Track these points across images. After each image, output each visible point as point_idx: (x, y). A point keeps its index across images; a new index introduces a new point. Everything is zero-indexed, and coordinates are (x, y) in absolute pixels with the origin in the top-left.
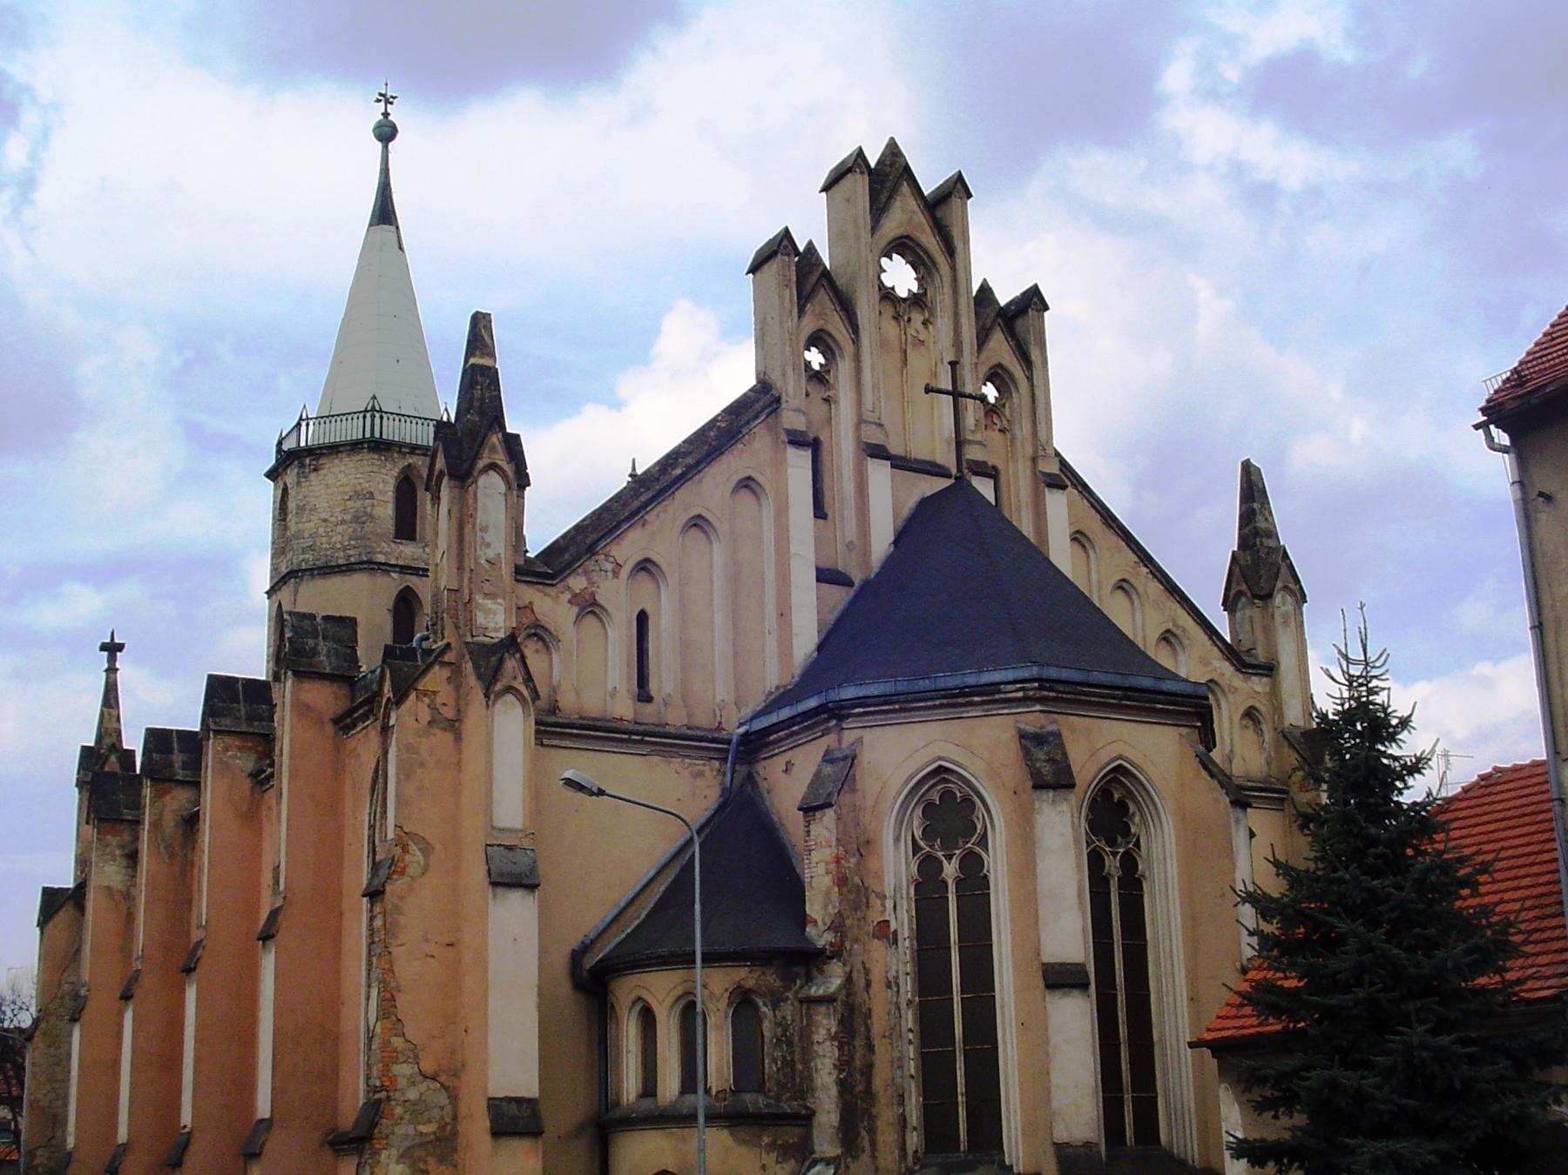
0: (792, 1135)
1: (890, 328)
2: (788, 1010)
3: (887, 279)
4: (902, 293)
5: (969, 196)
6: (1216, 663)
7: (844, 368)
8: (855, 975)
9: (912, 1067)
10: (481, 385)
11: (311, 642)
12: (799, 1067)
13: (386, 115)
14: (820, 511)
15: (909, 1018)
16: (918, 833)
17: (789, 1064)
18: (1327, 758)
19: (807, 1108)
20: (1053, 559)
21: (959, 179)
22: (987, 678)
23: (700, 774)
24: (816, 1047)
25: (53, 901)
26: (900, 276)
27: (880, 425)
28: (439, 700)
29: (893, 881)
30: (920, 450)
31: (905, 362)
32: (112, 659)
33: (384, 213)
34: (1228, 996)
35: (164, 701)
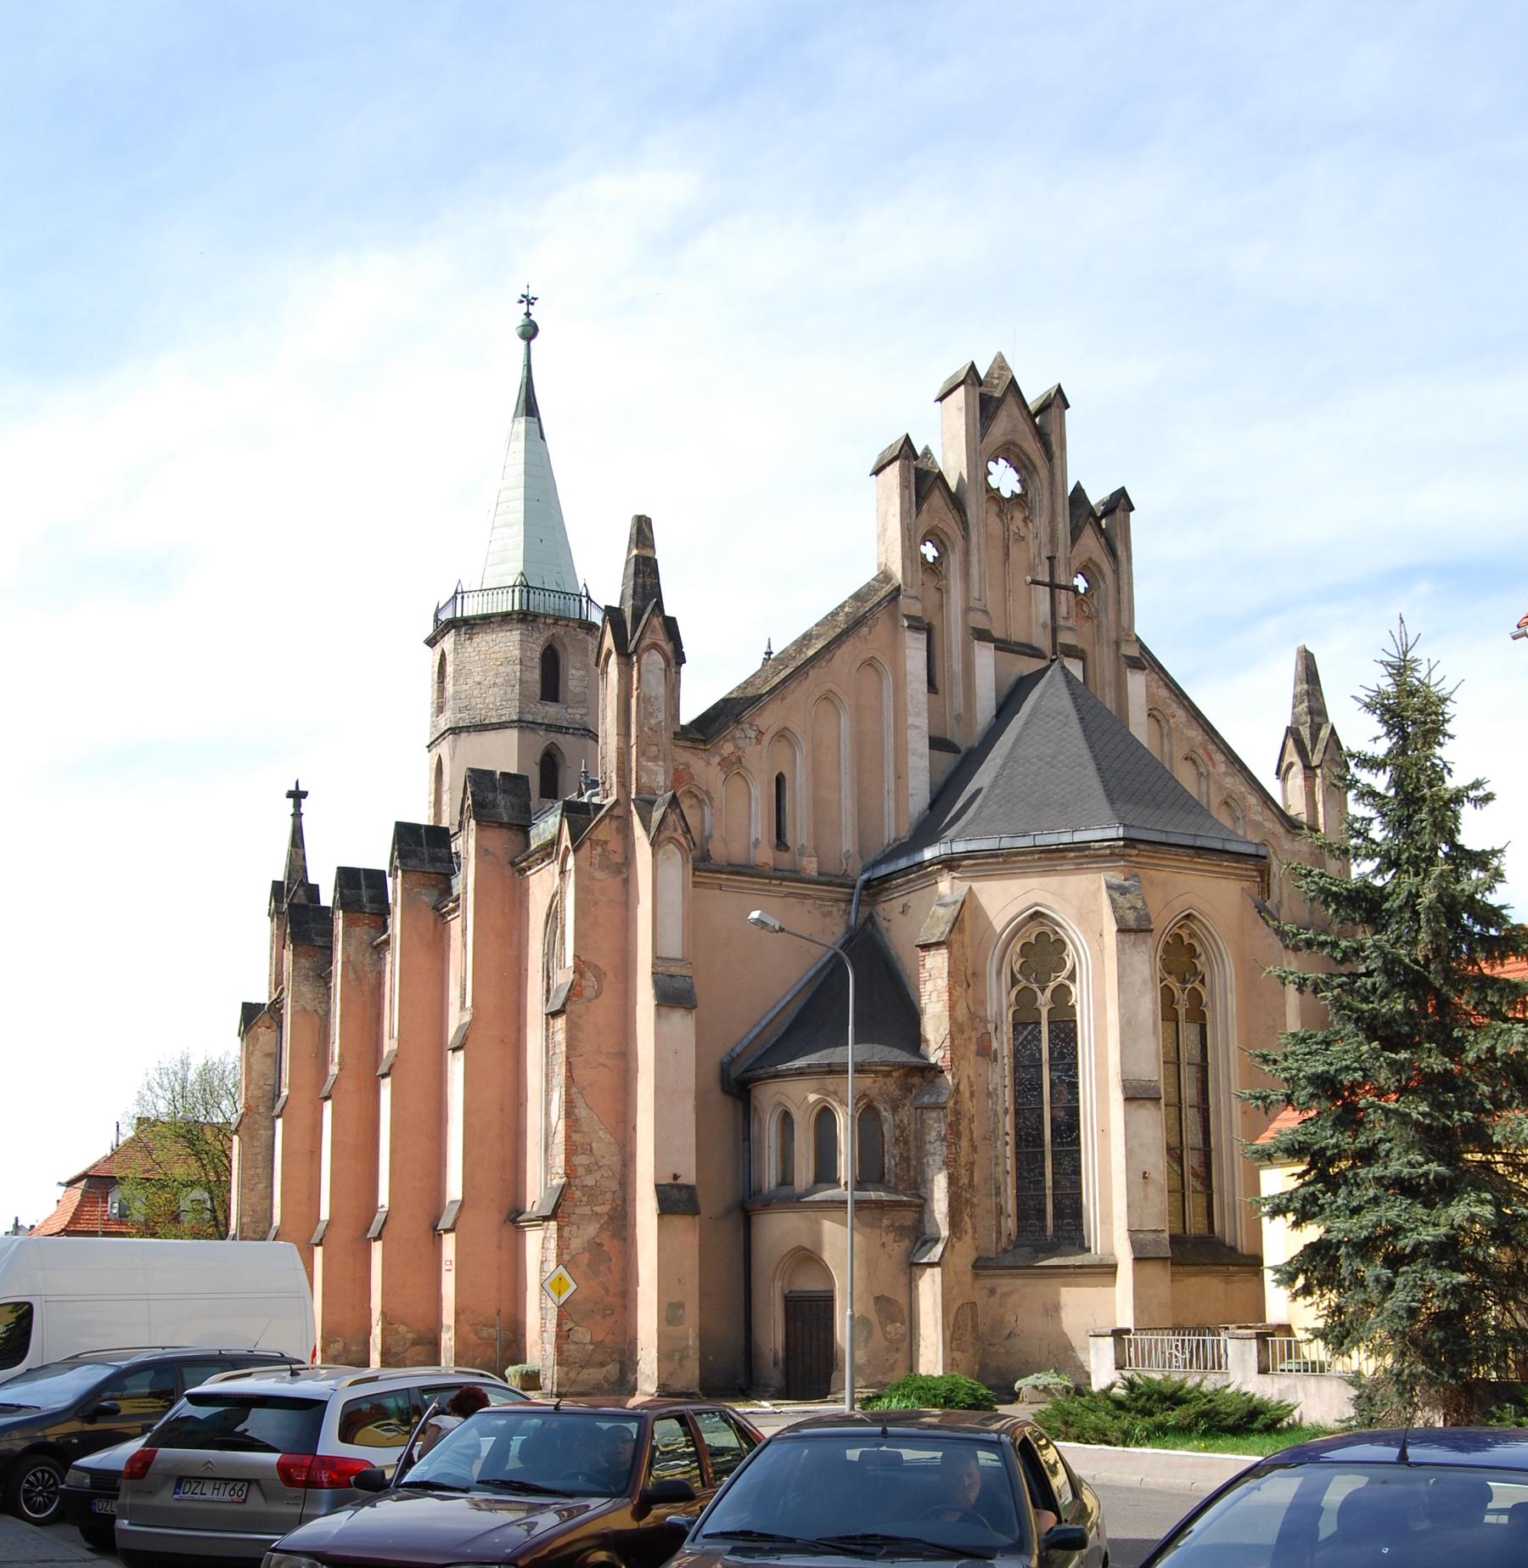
0: (908, 1218)
1: (995, 525)
2: (905, 1114)
3: (993, 481)
4: (1006, 494)
5: (1067, 406)
6: (1268, 825)
7: (954, 562)
8: (962, 1087)
9: (1010, 1164)
10: (644, 573)
11: (491, 796)
12: (914, 1163)
13: (528, 314)
14: (932, 685)
15: (1008, 1124)
16: (1016, 968)
17: (905, 1159)
18: (1442, 1169)
19: (920, 1197)
20: (1132, 729)
21: (1122, 493)
22: (1078, 837)
23: (829, 914)
24: (928, 1146)
25: (250, 1013)
26: (1004, 478)
27: (985, 612)
28: (610, 847)
29: (995, 1008)
30: (1018, 635)
31: (1007, 555)
32: (297, 806)
33: (529, 407)
34: (1448, 727)
35: (350, 840)
